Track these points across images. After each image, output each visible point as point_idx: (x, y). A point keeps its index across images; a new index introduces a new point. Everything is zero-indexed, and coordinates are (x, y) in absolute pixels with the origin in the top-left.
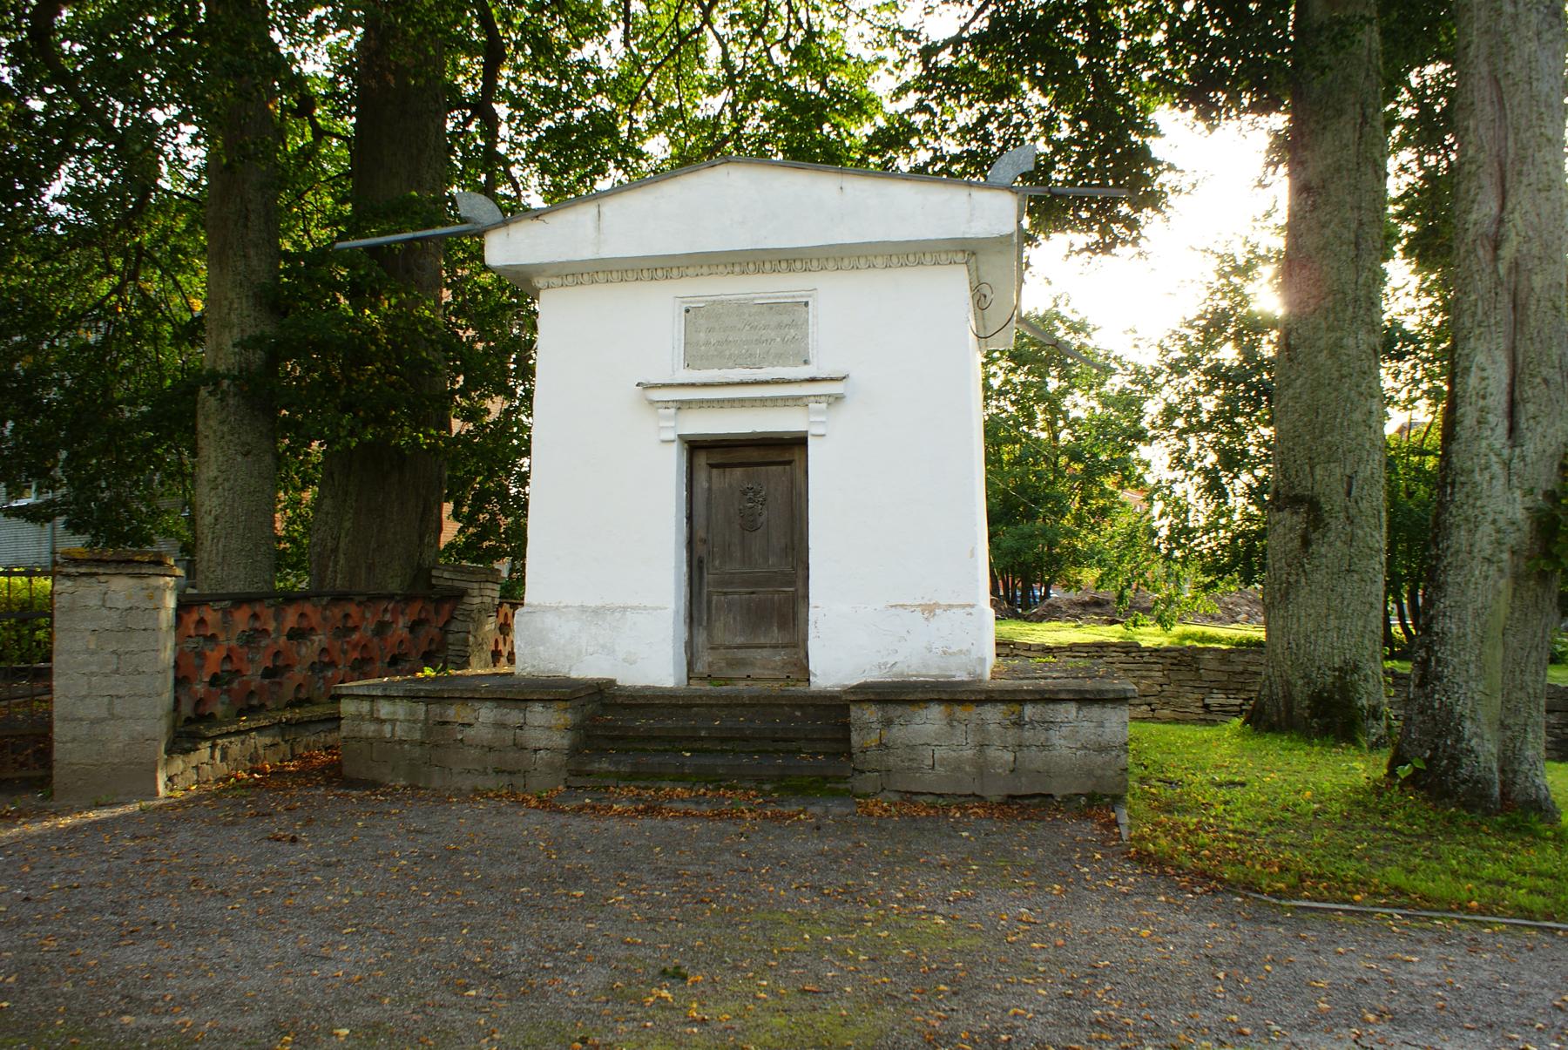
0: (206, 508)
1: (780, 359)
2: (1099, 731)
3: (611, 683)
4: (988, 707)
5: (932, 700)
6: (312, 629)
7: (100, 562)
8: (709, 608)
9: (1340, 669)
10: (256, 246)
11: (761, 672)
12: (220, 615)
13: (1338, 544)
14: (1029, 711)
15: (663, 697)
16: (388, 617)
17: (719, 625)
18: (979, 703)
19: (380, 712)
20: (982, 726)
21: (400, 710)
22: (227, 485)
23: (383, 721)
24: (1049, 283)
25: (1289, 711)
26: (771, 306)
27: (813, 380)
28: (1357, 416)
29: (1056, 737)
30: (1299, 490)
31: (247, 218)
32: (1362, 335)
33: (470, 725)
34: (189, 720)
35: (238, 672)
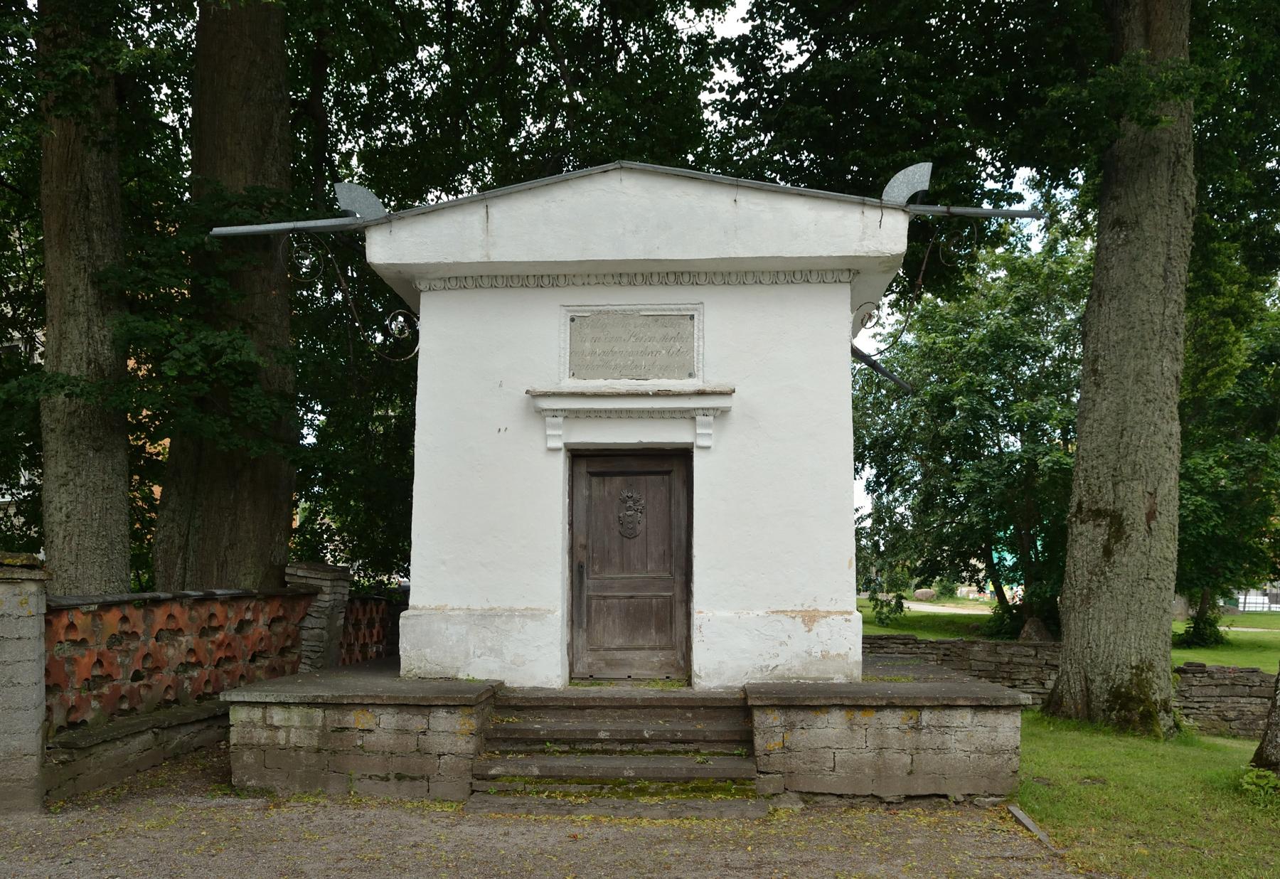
0: (56, 503)
1: (665, 371)
2: (993, 735)
3: (501, 684)
4: (887, 713)
5: (834, 706)
6: (180, 630)
8: (589, 612)
9: (1137, 667)
10: (100, 229)
11: (638, 672)
12: (90, 617)
13: (1138, 554)
14: (926, 716)
15: (556, 699)
16: (249, 616)
17: (599, 627)
18: (879, 708)
19: (268, 718)
20: (880, 732)
21: (296, 716)
22: (78, 481)
23: (277, 728)
25: (1088, 704)
27: (701, 394)
28: (1159, 439)
29: (951, 740)
30: (1101, 505)
31: (87, 199)
32: (1167, 363)
33: (370, 731)
34: (60, 729)
35: (109, 677)
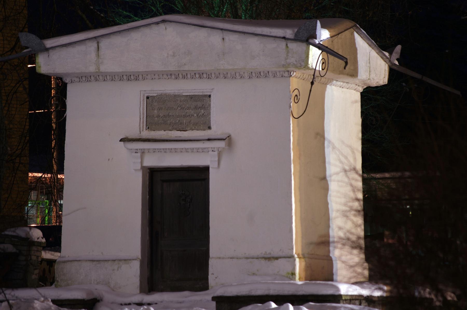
1: (196, 126)
7: (287, 277)
24: (223, 39)
26: (191, 97)
